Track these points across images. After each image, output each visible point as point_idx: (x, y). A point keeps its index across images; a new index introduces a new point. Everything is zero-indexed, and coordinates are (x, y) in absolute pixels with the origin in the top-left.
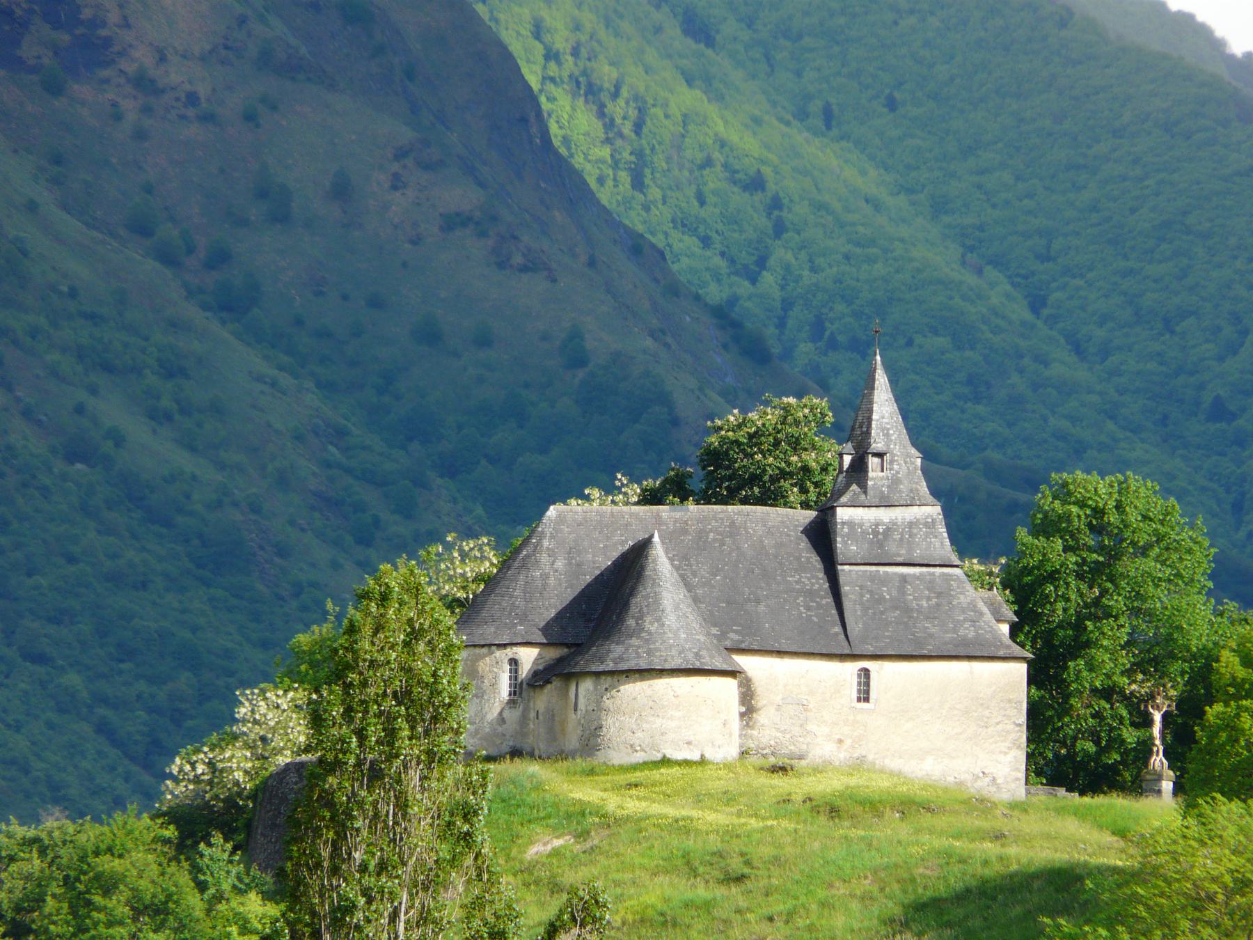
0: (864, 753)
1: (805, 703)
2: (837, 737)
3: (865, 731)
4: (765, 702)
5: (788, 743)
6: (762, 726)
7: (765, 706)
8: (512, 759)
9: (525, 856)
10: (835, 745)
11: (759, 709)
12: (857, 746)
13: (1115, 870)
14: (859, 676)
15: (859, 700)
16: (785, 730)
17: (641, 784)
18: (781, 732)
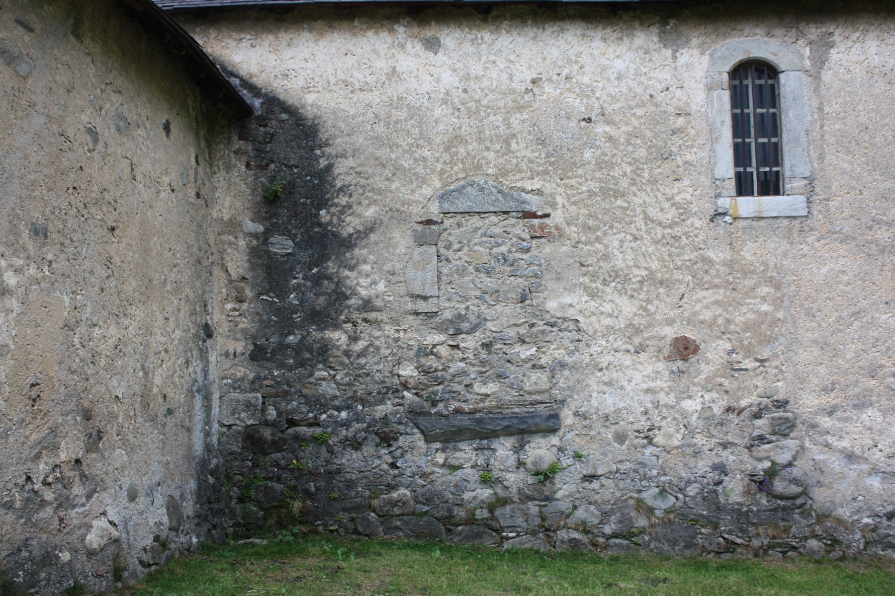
0: (781, 389)
1: (534, 203)
2: (670, 332)
3: (778, 303)
4: (370, 213)
5: (473, 372)
6: (367, 305)
7: (370, 229)
8: (845, 457)
9: (547, 458)
10: (661, 366)
11: (348, 244)
12: (749, 364)
13: (378, 405)
14: (738, 98)
15: (743, 187)
16: (460, 317)
17: (116, 526)
18: (441, 328)
